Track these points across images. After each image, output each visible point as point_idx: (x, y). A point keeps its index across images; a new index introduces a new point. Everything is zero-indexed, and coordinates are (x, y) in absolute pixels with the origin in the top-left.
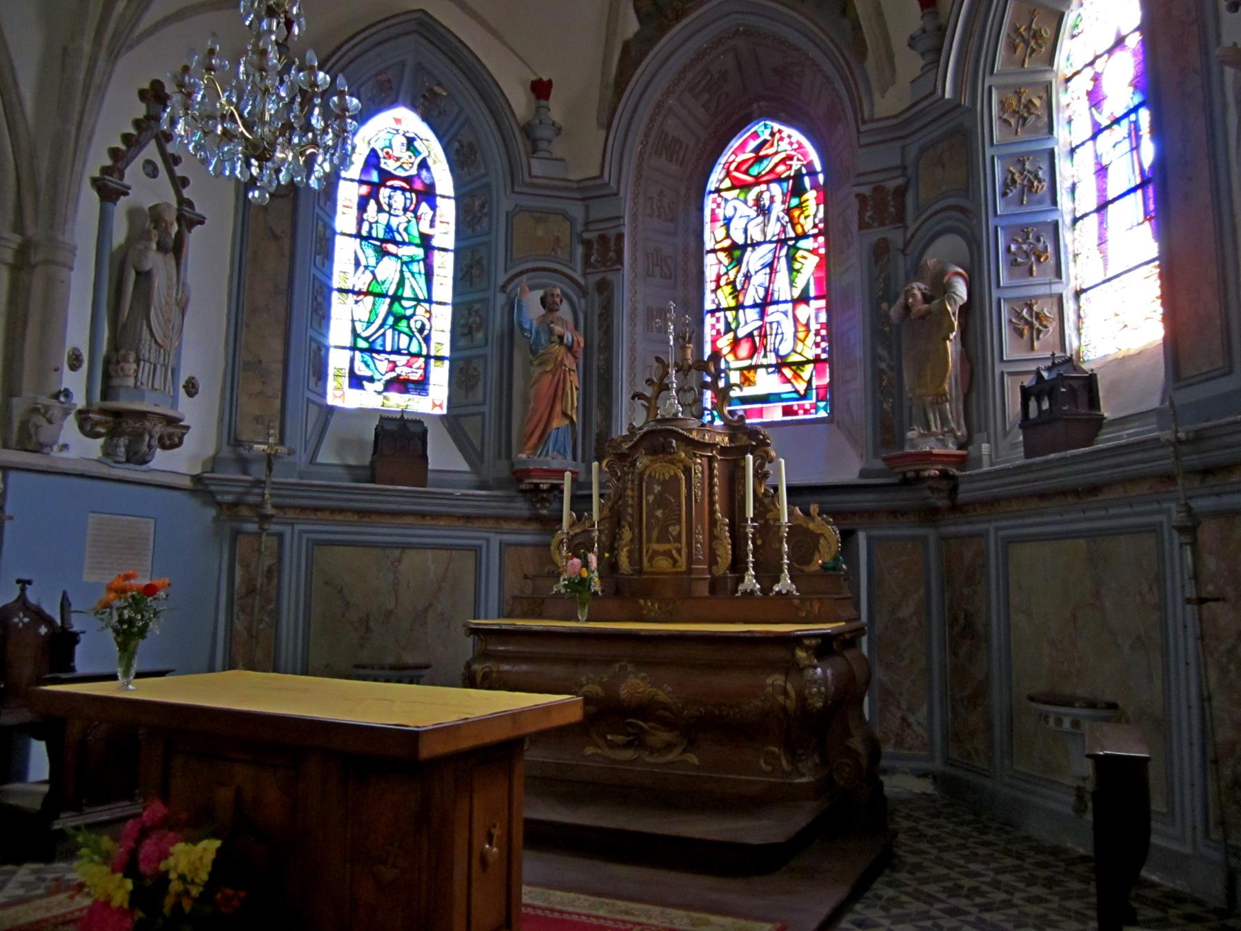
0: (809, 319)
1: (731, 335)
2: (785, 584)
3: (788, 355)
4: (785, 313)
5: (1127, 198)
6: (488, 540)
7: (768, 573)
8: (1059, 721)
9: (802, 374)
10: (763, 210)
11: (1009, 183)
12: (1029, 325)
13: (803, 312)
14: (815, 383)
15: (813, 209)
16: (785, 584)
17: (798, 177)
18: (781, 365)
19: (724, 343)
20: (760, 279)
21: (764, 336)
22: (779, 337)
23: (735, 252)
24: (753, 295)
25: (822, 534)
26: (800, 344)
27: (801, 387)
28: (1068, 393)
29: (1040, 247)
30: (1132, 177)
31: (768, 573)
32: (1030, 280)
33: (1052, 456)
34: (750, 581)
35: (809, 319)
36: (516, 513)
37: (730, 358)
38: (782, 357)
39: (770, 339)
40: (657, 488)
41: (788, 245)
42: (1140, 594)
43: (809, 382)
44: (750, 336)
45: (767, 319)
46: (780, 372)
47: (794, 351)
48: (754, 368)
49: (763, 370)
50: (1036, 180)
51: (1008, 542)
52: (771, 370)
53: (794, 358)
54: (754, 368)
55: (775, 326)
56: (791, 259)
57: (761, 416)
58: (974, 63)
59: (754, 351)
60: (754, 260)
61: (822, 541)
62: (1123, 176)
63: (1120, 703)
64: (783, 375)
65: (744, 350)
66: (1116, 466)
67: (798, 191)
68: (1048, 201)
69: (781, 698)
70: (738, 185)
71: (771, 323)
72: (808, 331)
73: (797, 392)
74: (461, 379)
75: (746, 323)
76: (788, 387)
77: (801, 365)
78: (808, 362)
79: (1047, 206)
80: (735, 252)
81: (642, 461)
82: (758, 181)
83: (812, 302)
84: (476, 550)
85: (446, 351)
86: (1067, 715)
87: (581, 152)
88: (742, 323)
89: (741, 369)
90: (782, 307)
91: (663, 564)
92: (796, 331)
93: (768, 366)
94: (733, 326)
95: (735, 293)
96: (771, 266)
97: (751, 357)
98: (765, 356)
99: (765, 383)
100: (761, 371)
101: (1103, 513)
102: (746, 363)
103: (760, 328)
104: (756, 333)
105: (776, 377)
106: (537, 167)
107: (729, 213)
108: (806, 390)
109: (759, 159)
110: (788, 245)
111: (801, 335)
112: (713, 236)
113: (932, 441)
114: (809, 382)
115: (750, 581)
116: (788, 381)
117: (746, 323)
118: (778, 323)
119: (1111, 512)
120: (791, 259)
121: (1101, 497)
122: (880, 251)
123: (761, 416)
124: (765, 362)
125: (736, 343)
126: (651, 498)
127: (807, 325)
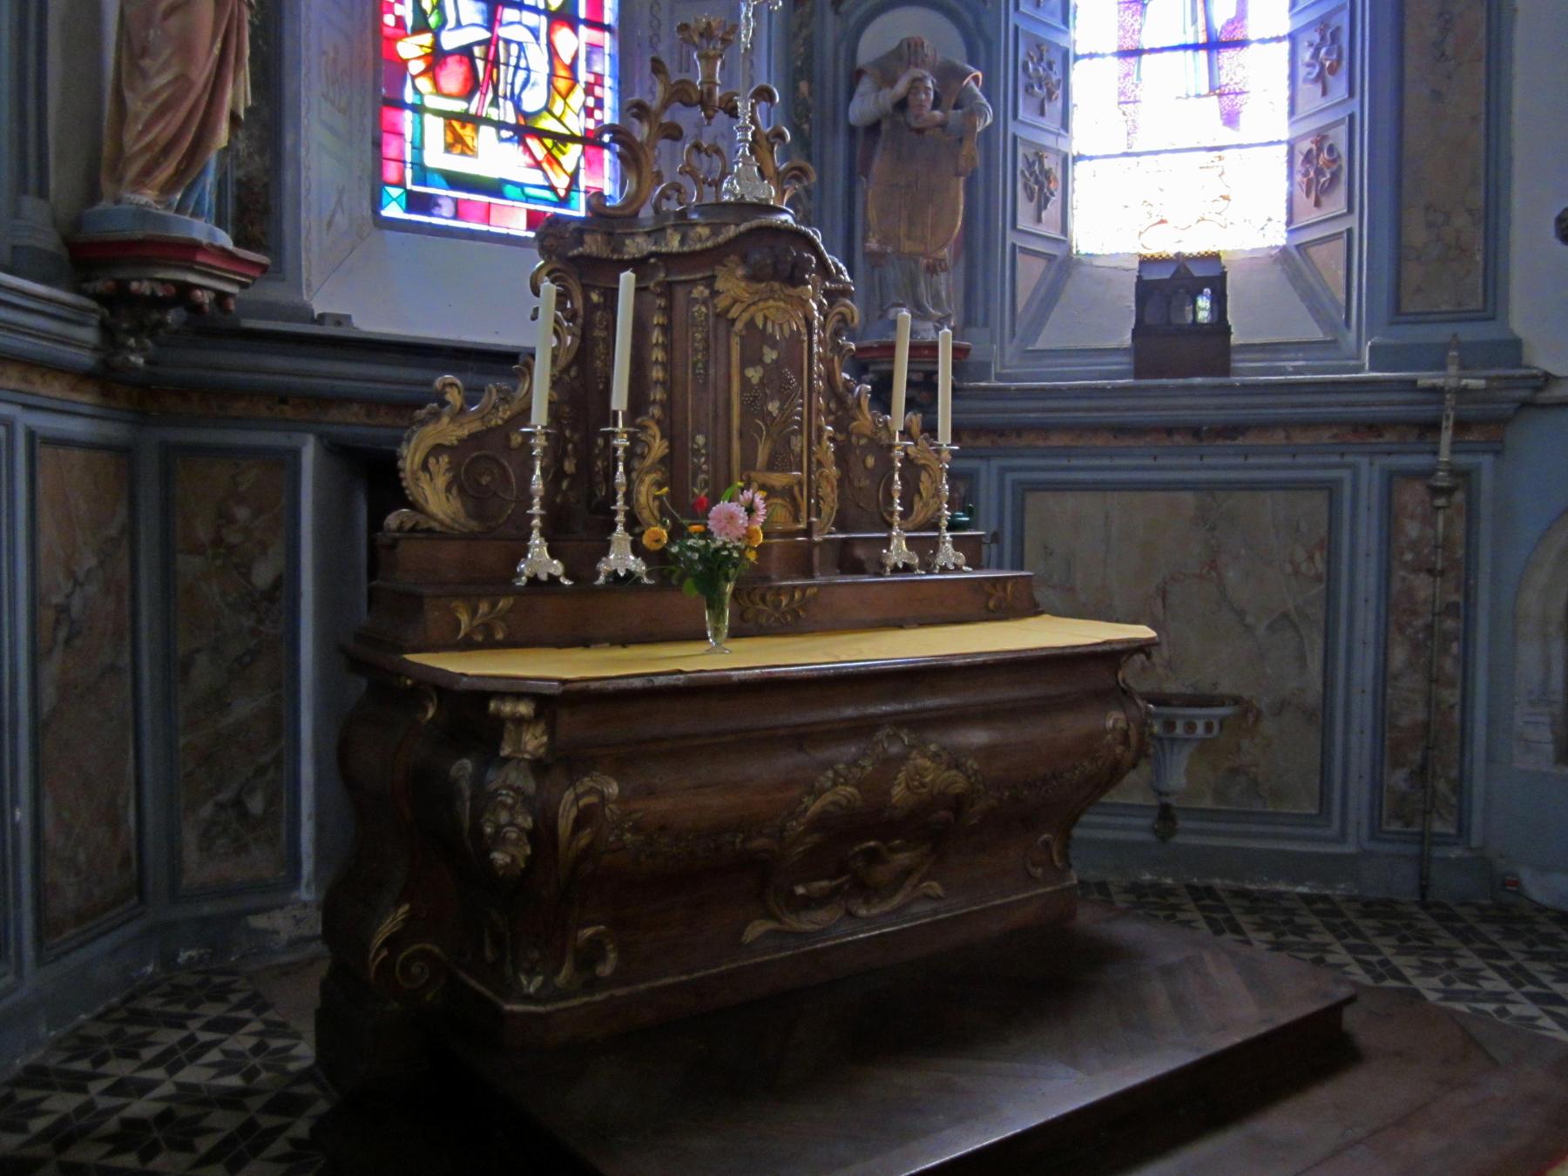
0: (575, 58)
1: (427, 39)
3: (537, 114)
4: (534, 32)
5: (1181, 53)
6: (1354, 468)
7: (580, 522)
8: (1190, 727)
9: (561, 158)
14: (583, 181)
18: (524, 130)
21: (493, 63)
22: (521, 75)
25: (924, 467)
26: (559, 101)
27: (561, 182)
30: (1190, 30)
32: (1040, 122)
33: (1198, 380)
35: (575, 58)
36: (68, 353)
37: (424, 84)
38: (526, 115)
39: (505, 75)
40: (770, 355)
42: (1292, 562)
43: (574, 178)
44: (465, 52)
45: (502, 32)
46: (522, 142)
47: (547, 109)
48: (476, 121)
49: (492, 130)
51: (1026, 488)
52: (506, 134)
53: (547, 123)
54: (476, 121)
55: (514, 49)
57: (487, 220)
59: (471, 87)
61: (924, 476)
64: (527, 149)
65: (453, 77)
66: (1347, 405)
68: (1059, 16)
69: (1119, 750)
71: (508, 42)
72: (574, 80)
73: (552, 188)
75: (459, 25)
76: (536, 177)
77: (562, 139)
78: (572, 138)
79: (1057, 22)
81: (732, 283)
83: (582, 28)
84: (1331, 489)
86: (1200, 717)
88: (451, 23)
89: (448, 116)
90: (530, 19)
92: (552, 75)
93: (500, 125)
94: (433, 21)
97: (467, 96)
98: (495, 103)
99: (494, 157)
100: (487, 132)
101: (1240, 460)
102: (458, 106)
103: (486, 43)
104: (477, 51)
105: (514, 150)
108: (568, 190)
111: (562, 84)
114: (574, 178)
116: (538, 165)
117: (459, 25)
118: (520, 44)
119: (1251, 461)
121: (1240, 441)
123: (486, 219)
124: (493, 114)
125: (436, 59)
126: (754, 374)
127: (572, 68)
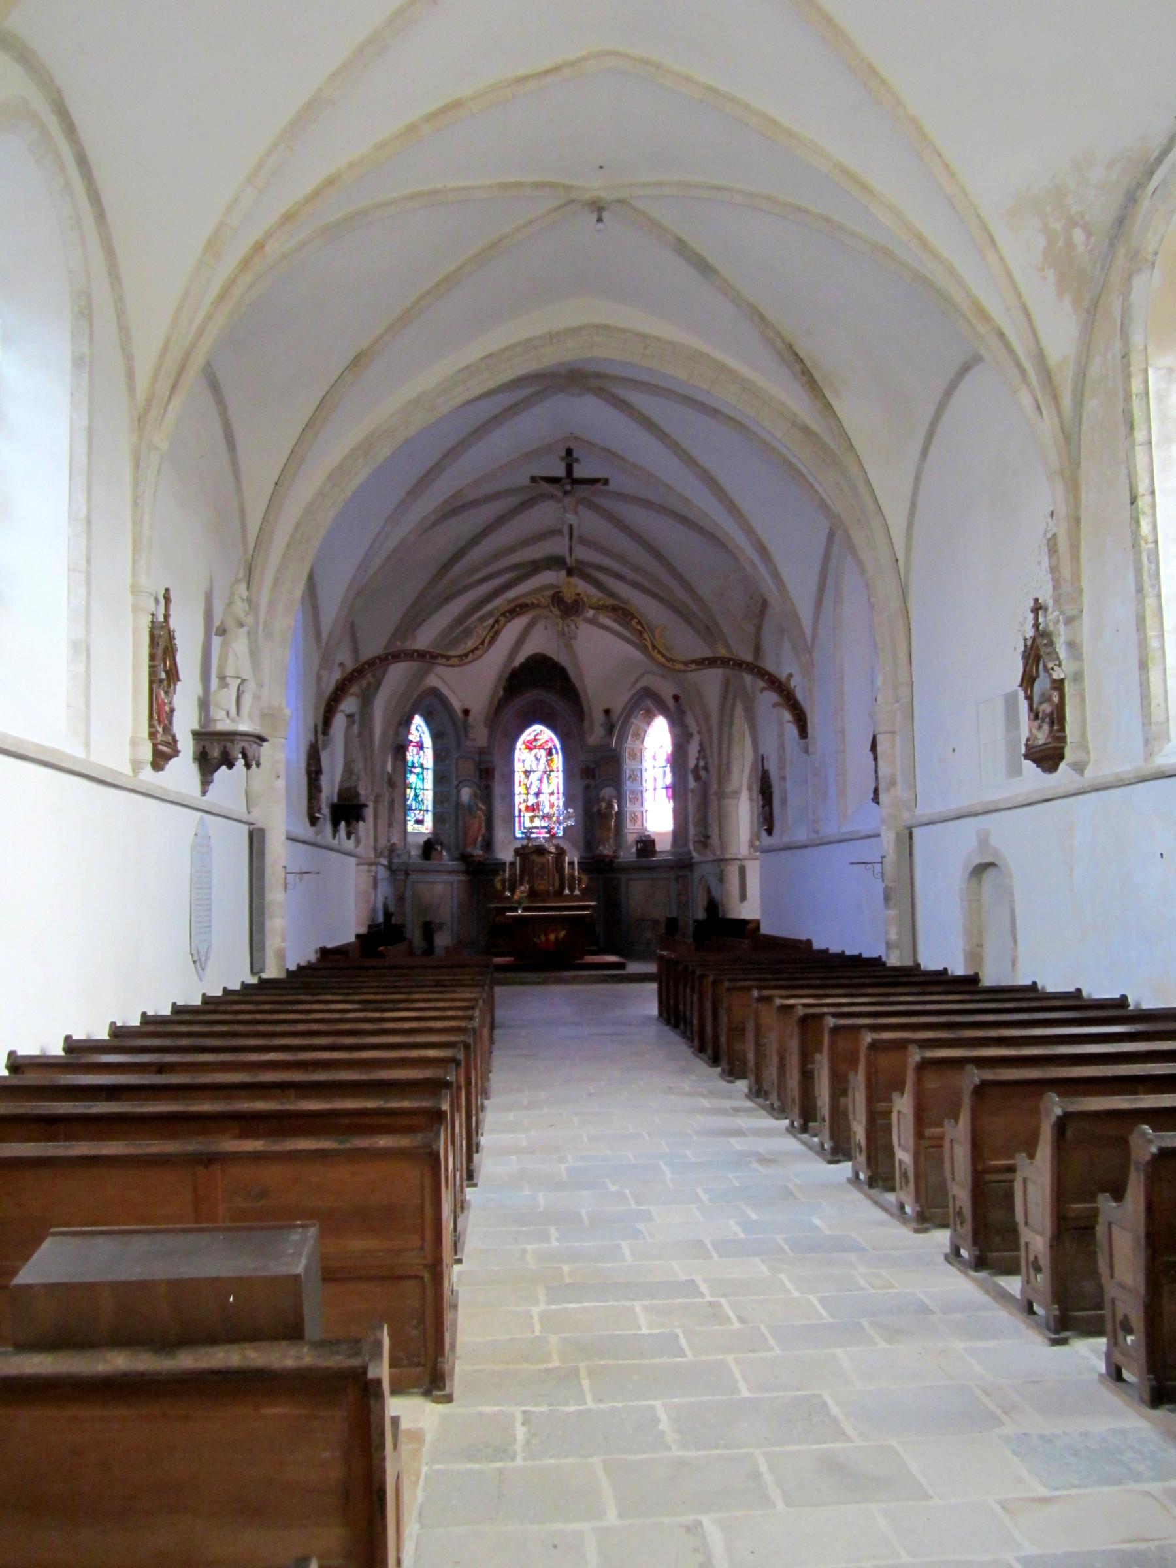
2: (577, 892)
7: (572, 889)
10: (538, 759)
11: (630, 777)
12: (634, 820)
13: (553, 799)
15: (558, 760)
16: (577, 892)
17: (550, 749)
19: (523, 807)
20: (536, 784)
23: (527, 773)
24: (534, 790)
28: (646, 845)
29: (638, 797)
31: (572, 889)
34: (567, 892)
41: (547, 773)
50: (637, 777)
56: (548, 778)
58: (622, 739)
60: (534, 777)
62: (661, 784)
63: (746, 903)
67: (550, 753)
70: (530, 749)
74: (437, 819)
80: (527, 773)
82: (535, 747)
85: (430, 808)
87: (479, 735)
91: (542, 887)
95: (527, 789)
96: (541, 780)
106: (469, 743)
107: (523, 758)
109: (536, 740)
110: (547, 773)
112: (518, 767)
113: (606, 850)
115: (567, 892)
120: (548, 778)
122: (587, 787)
